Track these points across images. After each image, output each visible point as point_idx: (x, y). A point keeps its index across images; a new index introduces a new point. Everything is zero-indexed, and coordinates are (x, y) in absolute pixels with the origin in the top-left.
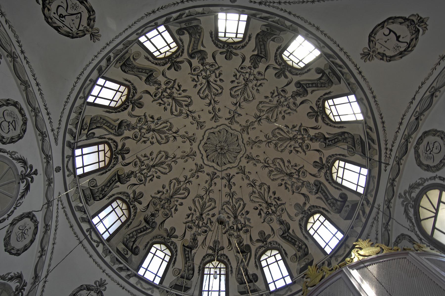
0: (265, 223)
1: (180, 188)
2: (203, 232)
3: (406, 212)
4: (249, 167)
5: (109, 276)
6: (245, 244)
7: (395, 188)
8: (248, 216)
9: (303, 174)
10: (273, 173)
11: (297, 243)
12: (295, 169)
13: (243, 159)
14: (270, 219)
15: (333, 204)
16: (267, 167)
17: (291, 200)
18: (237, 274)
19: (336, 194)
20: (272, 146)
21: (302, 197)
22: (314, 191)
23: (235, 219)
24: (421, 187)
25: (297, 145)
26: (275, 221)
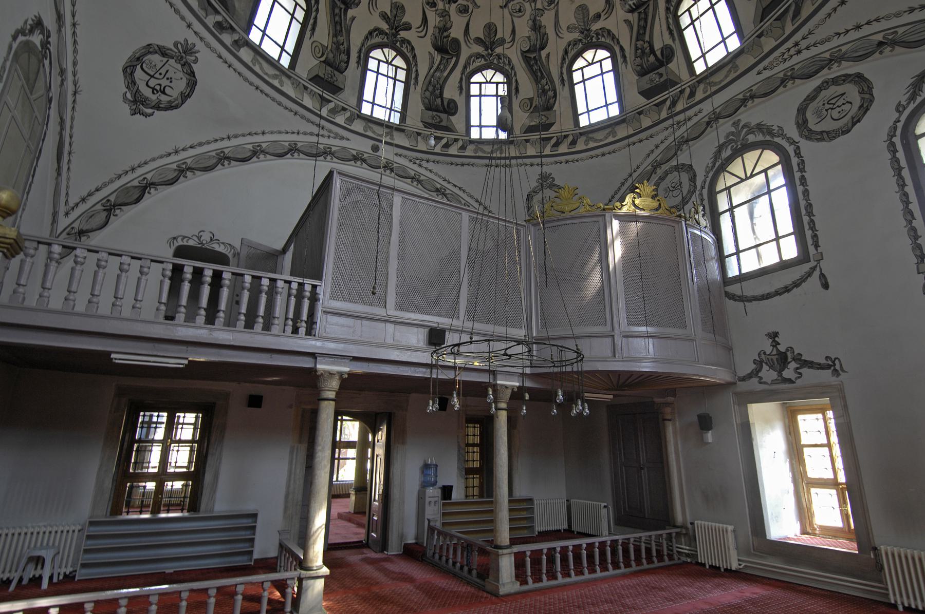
3: (721, 148)
5: (201, 39)
6: (452, 35)
7: (742, 108)
11: (544, 82)
14: (518, 7)
15: (643, 52)
19: (660, 39)
24: (768, 138)
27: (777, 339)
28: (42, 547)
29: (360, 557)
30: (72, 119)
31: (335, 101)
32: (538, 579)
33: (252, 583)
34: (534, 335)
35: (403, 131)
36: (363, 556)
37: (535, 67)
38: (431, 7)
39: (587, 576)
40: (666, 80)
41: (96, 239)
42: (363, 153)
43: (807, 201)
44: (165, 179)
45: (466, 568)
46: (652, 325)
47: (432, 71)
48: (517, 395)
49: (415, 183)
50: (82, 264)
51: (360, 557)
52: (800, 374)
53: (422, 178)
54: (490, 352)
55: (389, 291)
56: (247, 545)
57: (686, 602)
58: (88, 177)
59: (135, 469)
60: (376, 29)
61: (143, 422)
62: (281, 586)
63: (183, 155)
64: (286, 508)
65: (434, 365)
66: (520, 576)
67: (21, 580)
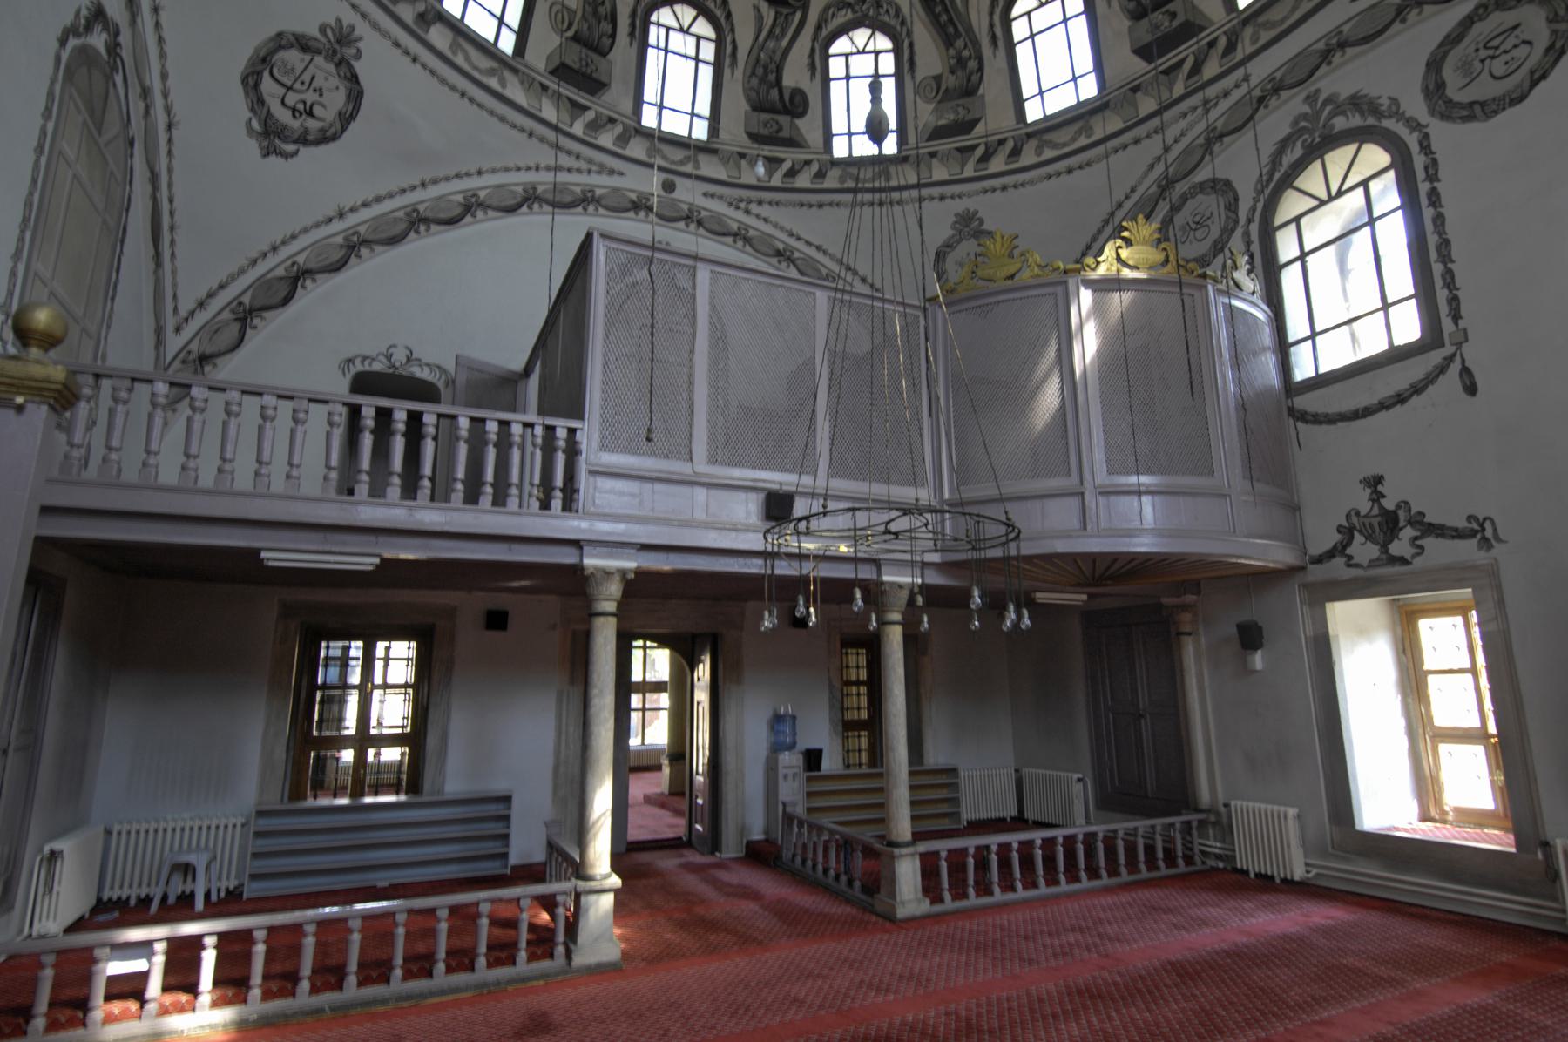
3: (1284, 145)
5: (364, 16)
7: (1324, 69)
11: (959, 43)
27: (1380, 488)
28: (190, 850)
30: (170, 170)
31: (597, 107)
32: (960, 894)
33: (500, 900)
34: (946, 496)
35: (714, 152)
36: (683, 860)
37: (944, 18)
39: (1043, 889)
40: (1182, 25)
41: (227, 369)
43: (1440, 234)
44: (327, 262)
45: (844, 878)
46: (1149, 472)
47: (761, 38)
49: (740, 244)
50: (203, 410)
52: (1422, 548)
53: (752, 233)
55: (695, 433)
56: (498, 844)
58: (206, 268)
59: (320, 729)
61: (327, 658)
62: (548, 903)
63: (351, 220)
64: (556, 788)
66: (930, 886)
67: (165, 898)
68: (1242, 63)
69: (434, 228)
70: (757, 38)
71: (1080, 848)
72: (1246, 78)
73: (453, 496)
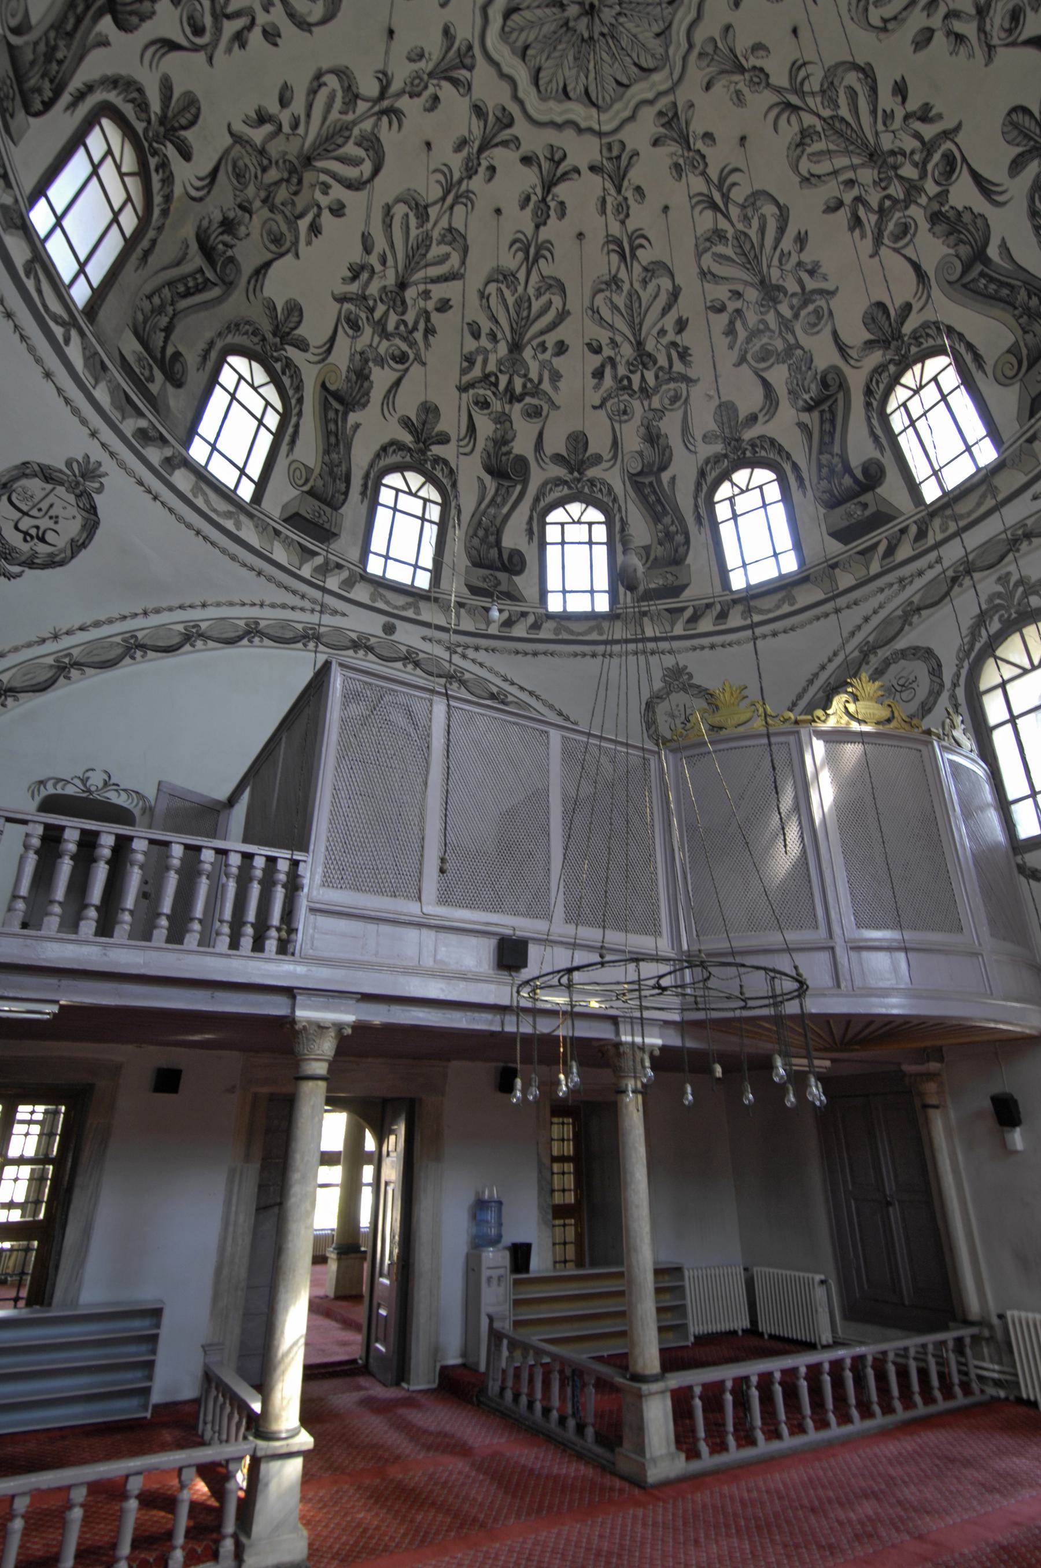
0: (602, 413)
1: (348, 127)
2: (394, 358)
3: (982, 619)
4: (652, 168)
5: (112, 454)
8: (557, 362)
9: (813, 319)
10: (720, 249)
11: (667, 520)
12: (801, 283)
13: (648, 114)
15: (832, 472)
16: (714, 207)
17: (722, 379)
18: (471, 533)
20: (789, 130)
21: (759, 392)
22: (806, 397)
23: (511, 351)
25: (874, 198)
26: (637, 420)
29: (356, 1396)
34: (685, 947)
36: (362, 1394)
38: (482, 408)
40: (873, 515)
42: (367, 637)
44: (34, 682)
45: (571, 1423)
47: (483, 506)
48: (665, 1061)
51: (356, 1396)
54: (611, 984)
57: (1026, 1494)
60: (392, 443)
63: (66, 642)
64: (216, 1296)
65: (526, 1010)
66: (684, 1440)
68: (937, 545)
69: (151, 654)
70: (480, 504)
71: (848, 1375)
72: (939, 560)
73: (156, 932)
